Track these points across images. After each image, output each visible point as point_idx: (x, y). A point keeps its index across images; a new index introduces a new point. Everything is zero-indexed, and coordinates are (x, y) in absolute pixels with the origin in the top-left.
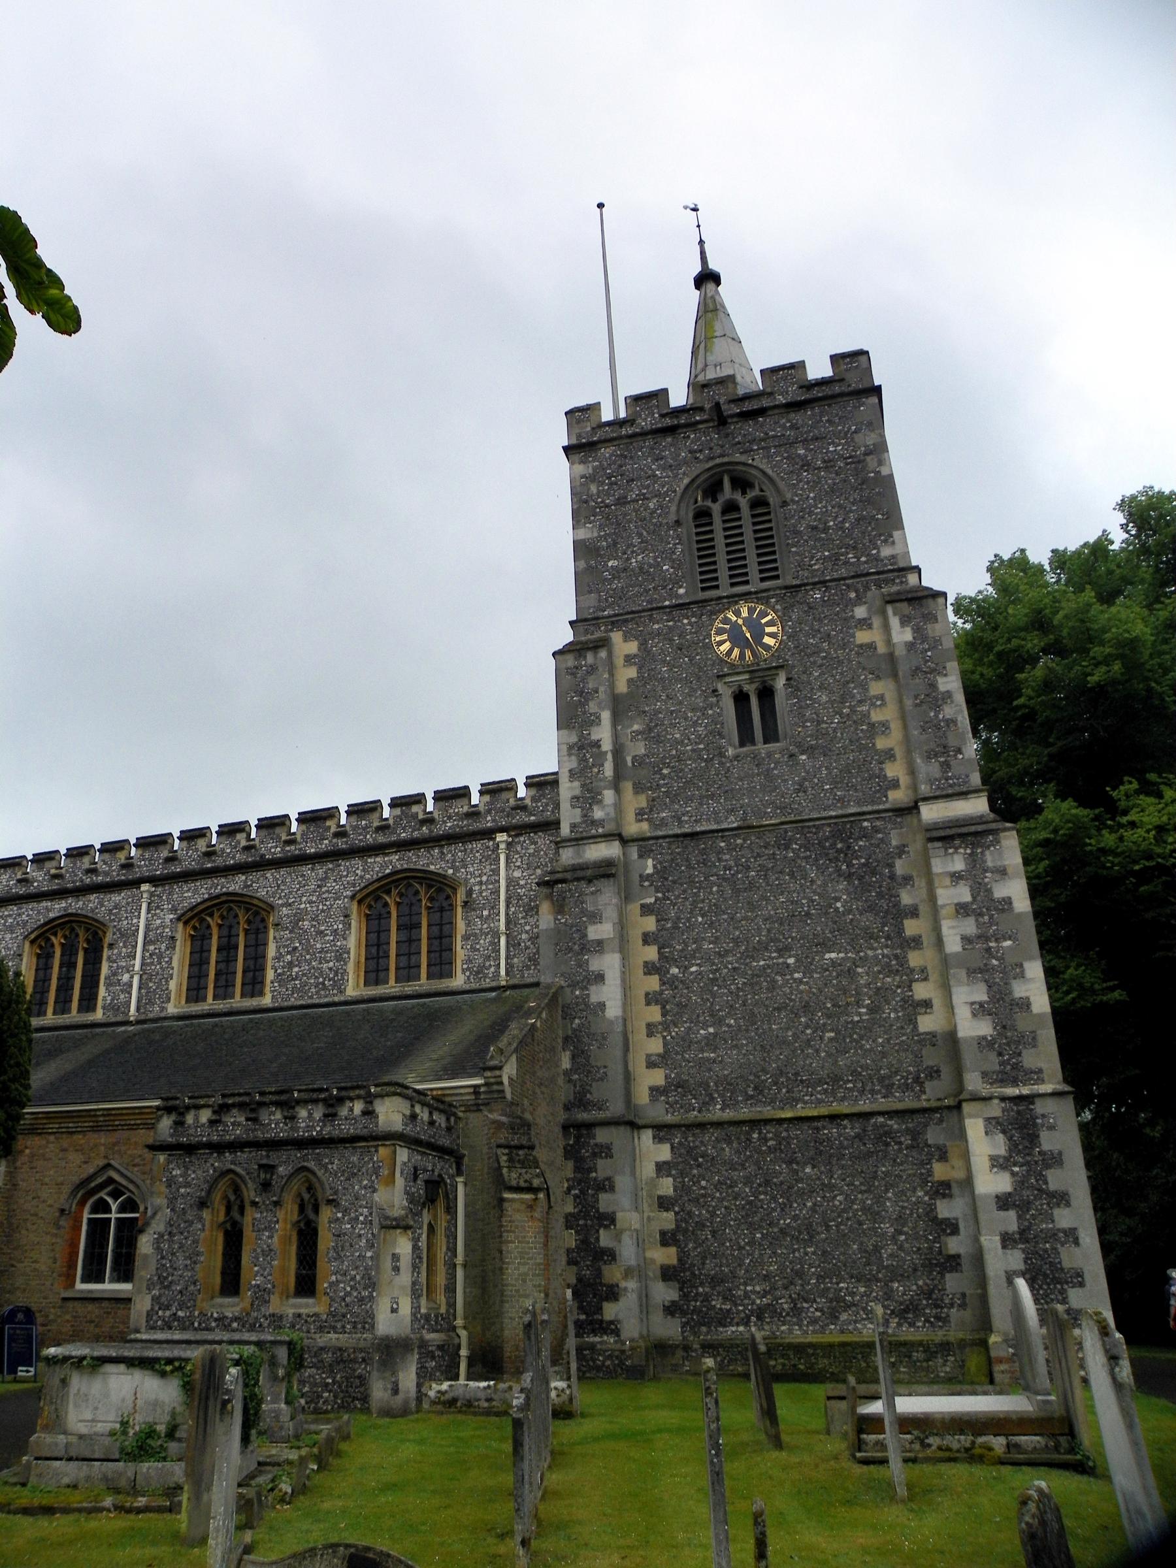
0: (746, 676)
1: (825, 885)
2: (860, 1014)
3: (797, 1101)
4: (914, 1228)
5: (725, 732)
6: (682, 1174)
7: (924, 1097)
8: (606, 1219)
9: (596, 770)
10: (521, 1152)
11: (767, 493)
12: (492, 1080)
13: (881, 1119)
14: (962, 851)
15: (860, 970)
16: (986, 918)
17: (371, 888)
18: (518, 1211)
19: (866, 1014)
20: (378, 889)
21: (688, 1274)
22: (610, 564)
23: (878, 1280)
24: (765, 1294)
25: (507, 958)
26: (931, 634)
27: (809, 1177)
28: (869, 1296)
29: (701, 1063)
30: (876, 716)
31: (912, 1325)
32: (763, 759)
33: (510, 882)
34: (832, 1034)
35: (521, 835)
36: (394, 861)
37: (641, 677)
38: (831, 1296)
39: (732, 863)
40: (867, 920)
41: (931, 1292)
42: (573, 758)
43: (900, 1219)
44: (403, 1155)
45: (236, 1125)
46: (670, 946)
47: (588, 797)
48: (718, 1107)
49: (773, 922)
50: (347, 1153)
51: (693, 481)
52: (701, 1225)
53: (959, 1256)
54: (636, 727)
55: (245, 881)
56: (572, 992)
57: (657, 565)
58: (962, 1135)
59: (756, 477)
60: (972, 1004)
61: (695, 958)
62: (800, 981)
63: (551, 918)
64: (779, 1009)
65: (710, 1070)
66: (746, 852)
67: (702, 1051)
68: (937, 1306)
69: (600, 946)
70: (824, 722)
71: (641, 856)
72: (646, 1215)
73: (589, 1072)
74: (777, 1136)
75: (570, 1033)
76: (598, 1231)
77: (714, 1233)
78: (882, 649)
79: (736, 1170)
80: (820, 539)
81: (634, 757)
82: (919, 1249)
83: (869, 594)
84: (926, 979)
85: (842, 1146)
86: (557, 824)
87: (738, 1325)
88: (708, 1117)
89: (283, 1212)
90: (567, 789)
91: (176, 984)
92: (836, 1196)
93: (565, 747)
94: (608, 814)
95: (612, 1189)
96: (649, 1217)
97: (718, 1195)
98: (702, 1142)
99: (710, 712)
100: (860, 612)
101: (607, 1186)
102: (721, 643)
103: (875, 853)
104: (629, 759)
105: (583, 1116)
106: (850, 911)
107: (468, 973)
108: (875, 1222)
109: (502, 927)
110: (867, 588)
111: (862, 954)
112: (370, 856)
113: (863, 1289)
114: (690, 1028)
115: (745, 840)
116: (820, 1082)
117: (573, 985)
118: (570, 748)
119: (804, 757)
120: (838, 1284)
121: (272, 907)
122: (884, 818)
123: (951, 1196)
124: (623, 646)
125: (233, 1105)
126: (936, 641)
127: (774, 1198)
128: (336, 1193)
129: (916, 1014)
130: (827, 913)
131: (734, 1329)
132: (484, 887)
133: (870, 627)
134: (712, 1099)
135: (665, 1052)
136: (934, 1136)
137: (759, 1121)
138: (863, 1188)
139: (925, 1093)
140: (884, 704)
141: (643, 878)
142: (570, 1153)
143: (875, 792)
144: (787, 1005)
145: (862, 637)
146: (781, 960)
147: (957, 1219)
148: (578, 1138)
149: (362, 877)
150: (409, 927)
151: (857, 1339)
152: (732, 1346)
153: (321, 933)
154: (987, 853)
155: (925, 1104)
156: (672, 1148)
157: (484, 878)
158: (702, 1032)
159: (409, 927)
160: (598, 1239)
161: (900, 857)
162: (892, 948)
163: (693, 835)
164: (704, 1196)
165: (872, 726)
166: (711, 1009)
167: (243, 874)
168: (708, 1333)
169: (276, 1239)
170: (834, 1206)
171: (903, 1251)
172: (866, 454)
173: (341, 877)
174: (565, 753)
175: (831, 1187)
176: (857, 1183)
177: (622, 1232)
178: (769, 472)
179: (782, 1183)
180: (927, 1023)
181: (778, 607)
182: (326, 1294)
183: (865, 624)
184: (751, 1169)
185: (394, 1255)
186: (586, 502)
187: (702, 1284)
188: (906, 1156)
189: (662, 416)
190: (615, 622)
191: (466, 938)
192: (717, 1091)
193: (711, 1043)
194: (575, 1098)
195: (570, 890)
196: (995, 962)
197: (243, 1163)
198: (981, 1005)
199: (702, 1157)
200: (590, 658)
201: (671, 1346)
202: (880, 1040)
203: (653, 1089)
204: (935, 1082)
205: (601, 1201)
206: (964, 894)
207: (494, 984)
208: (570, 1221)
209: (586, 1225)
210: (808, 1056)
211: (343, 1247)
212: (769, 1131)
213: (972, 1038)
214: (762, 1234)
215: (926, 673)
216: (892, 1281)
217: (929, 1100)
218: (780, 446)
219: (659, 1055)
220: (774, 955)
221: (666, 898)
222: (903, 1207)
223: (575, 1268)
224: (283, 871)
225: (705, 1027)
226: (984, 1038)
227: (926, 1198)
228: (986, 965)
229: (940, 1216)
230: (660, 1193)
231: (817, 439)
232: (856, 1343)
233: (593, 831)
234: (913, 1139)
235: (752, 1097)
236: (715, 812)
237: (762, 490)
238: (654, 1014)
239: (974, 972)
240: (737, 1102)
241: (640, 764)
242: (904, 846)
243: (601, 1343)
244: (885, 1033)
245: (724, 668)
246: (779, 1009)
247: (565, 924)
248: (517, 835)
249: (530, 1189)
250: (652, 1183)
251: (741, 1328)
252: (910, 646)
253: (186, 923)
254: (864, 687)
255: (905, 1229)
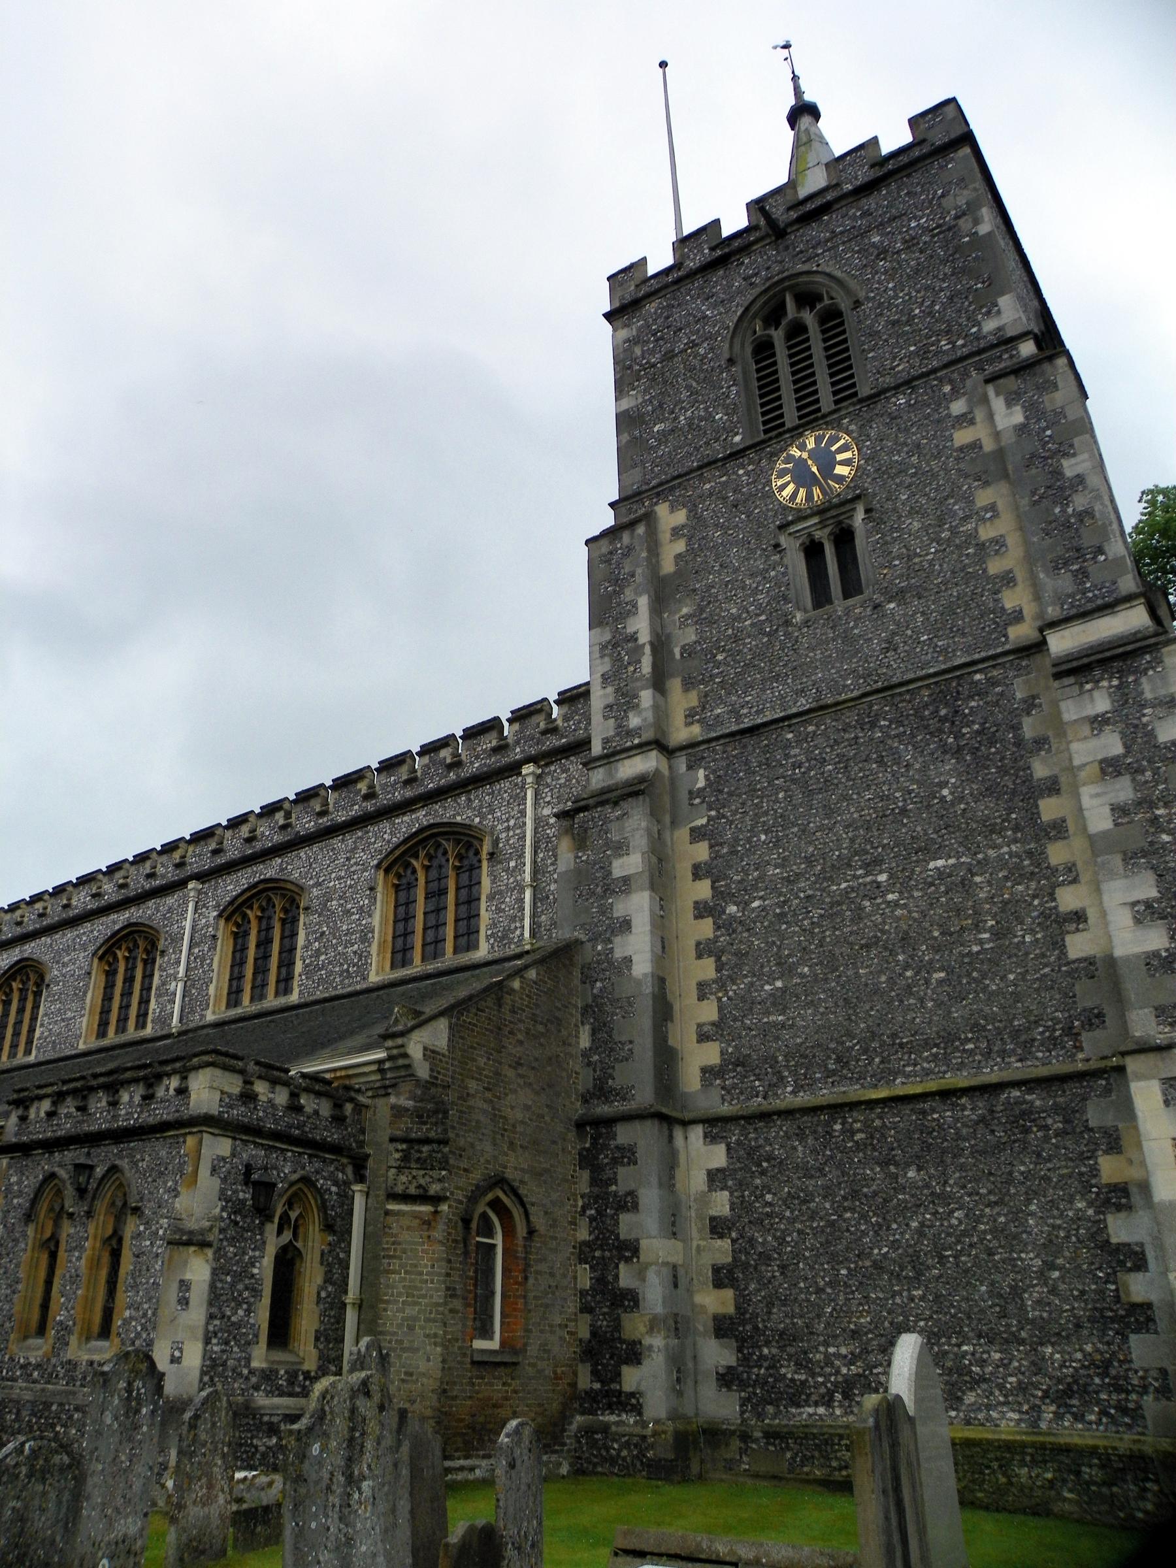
0: (815, 520)
1: (925, 768)
2: (981, 942)
3: (897, 1073)
4: (1072, 1260)
5: (791, 594)
6: (741, 1185)
7: (1080, 1056)
8: (627, 1249)
9: (632, 669)
10: (425, 1149)
11: (838, 300)
12: (395, 1052)
13: (1016, 1093)
14: (1105, 683)
15: (978, 879)
16: (1148, 773)
17: (397, 853)
18: (409, 1228)
19: (990, 940)
20: (404, 853)
21: (748, 1327)
22: (656, 429)
23: (1022, 1342)
24: (852, 1360)
25: (534, 915)
26: (1048, 406)
27: (913, 1184)
28: (1006, 1366)
29: (766, 1031)
30: (986, 533)
31: (1080, 1417)
32: (840, 618)
33: (538, 820)
34: (942, 975)
35: (552, 763)
36: (421, 817)
37: (690, 550)
38: (949, 1364)
39: (803, 758)
40: (983, 809)
41: (1107, 1364)
42: (607, 659)
43: (1050, 1246)
44: (223, 1146)
45: (68, 1121)
46: (726, 877)
47: (625, 702)
48: (789, 1089)
49: (857, 829)
50: (158, 1145)
51: (747, 309)
52: (765, 1258)
53: (1149, 1306)
54: (685, 611)
55: (281, 864)
56: (594, 947)
57: (709, 417)
58: (1127, 1109)
59: (824, 285)
60: (1134, 904)
61: (757, 889)
62: (896, 904)
63: (571, 856)
64: (867, 946)
65: (777, 1038)
66: (820, 740)
67: (767, 1013)
68: (1119, 1389)
69: (626, 884)
70: (917, 555)
71: (690, 768)
72: (695, 1244)
73: (612, 1050)
74: (867, 1125)
75: (590, 1001)
76: (617, 1267)
77: (783, 1268)
78: (988, 446)
79: (812, 1177)
80: (905, 333)
81: (683, 647)
82: (1083, 1293)
83: (969, 383)
84: (1075, 881)
85: (959, 1137)
86: (585, 743)
87: (816, 1404)
88: (778, 1104)
89: (94, 1224)
90: (599, 698)
91: (217, 988)
92: (952, 1212)
93: (597, 648)
94: (645, 720)
95: (635, 1207)
96: (698, 1246)
97: (788, 1214)
98: (766, 1139)
99: (773, 573)
100: (958, 407)
101: (629, 1203)
102: (782, 488)
103: (992, 713)
104: (677, 651)
105: (603, 1110)
106: (961, 799)
107: (492, 941)
108: (1012, 1251)
109: (528, 877)
110: (966, 375)
111: (980, 856)
112: (397, 816)
113: (997, 1356)
114: (752, 984)
115: (817, 726)
116: (927, 1045)
117: (594, 939)
118: (603, 647)
119: (892, 605)
120: (959, 1346)
121: (302, 888)
122: (1003, 665)
123: (1129, 1208)
124: (670, 517)
125: (68, 1093)
126: (1056, 414)
127: (864, 1217)
128: (141, 1199)
129: (1063, 933)
130: (929, 806)
131: (811, 1410)
132: (511, 833)
133: (972, 422)
134: (782, 1078)
135: (721, 1019)
136: (1096, 1115)
137: (842, 1106)
138: (992, 1198)
139: (1081, 1049)
140: (996, 515)
141: (692, 794)
142: (587, 1160)
143: (990, 633)
144: (878, 939)
145: (962, 437)
146: (869, 879)
147: (1142, 1245)
148: (595, 1140)
149: (389, 842)
150: (436, 894)
151: (990, 1436)
152: (806, 1436)
153: (348, 913)
154: (1144, 680)
155: (1080, 1066)
156: (729, 1149)
157: (512, 822)
158: (767, 987)
159: (436, 894)
160: (617, 1277)
161: (1029, 714)
162: (1023, 841)
163: (752, 730)
164: (768, 1215)
165: (981, 546)
166: (778, 955)
167: (279, 856)
168: (774, 1417)
169: (83, 1261)
170: (951, 1226)
171: (1057, 1295)
172: (957, 217)
173: (370, 844)
174: (598, 655)
175: (945, 1198)
176: (983, 1191)
177: (647, 1266)
178: (838, 274)
179: (875, 1194)
180: (1078, 946)
181: (853, 427)
182: (119, 1334)
183: (966, 420)
184: (833, 1174)
185: (182, 1282)
186: (630, 367)
187: (767, 1343)
188: (1057, 1147)
189: (712, 249)
190: (660, 491)
191: (491, 898)
192: (787, 1066)
193: (779, 1001)
194: (595, 1086)
195: (593, 818)
196: (1166, 838)
197: (61, 1164)
198: (1148, 904)
199: (767, 1161)
200: (626, 538)
201: (724, 1432)
202: (1011, 977)
203: (704, 1070)
204: (1097, 1033)
205: (621, 1225)
206: (1112, 744)
207: (518, 950)
208: (583, 1253)
209: (603, 1258)
210: (909, 1008)
211: (140, 1271)
212: (856, 1121)
213: (1137, 956)
214: (849, 1269)
215: (1046, 458)
216: (1042, 1344)
217: (1088, 1060)
218: (850, 240)
219: (713, 1024)
220: (860, 872)
221: (721, 816)
222: (1053, 1226)
223: (587, 1317)
224: (315, 848)
225: (771, 980)
226: (1156, 954)
227: (1090, 1212)
228: (1151, 843)
229: (1114, 1240)
230: (713, 1213)
231: (895, 218)
232: (989, 1442)
233: (629, 744)
234: (1066, 1121)
235: (833, 1073)
236: (781, 697)
237: (832, 298)
238: (707, 969)
239: (1135, 855)
240: (815, 1081)
241: (690, 655)
242: (1034, 697)
243: (617, 1424)
244: (1018, 965)
245: (788, 519)
246: (867, 946)
247: (586, 862)
248: (547, 765)
249: (423, 1197)
250: (703, 1200)
251: (821, 1410)
252: (1021, 429)
253: (228, 919)
254: (969, 500)
255: (1060, 1261)
